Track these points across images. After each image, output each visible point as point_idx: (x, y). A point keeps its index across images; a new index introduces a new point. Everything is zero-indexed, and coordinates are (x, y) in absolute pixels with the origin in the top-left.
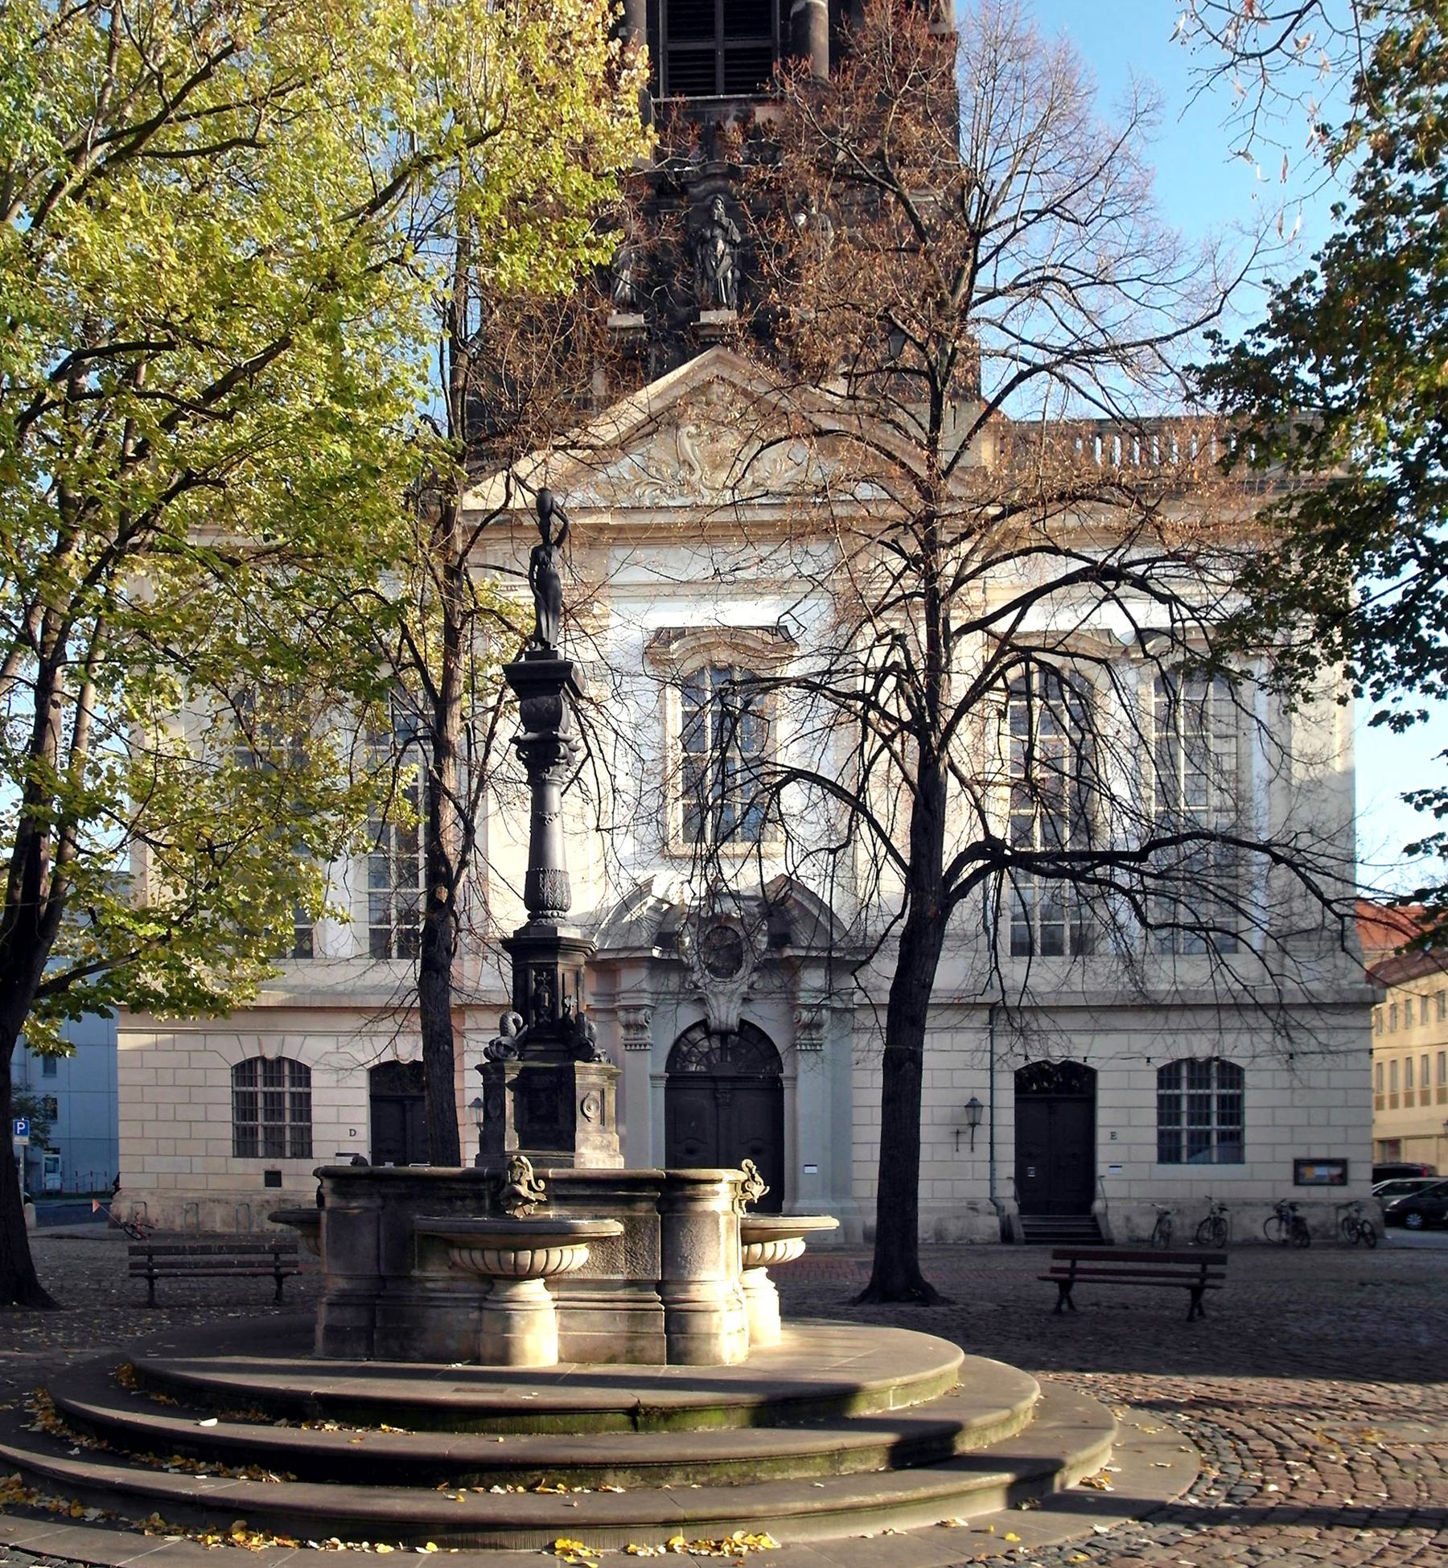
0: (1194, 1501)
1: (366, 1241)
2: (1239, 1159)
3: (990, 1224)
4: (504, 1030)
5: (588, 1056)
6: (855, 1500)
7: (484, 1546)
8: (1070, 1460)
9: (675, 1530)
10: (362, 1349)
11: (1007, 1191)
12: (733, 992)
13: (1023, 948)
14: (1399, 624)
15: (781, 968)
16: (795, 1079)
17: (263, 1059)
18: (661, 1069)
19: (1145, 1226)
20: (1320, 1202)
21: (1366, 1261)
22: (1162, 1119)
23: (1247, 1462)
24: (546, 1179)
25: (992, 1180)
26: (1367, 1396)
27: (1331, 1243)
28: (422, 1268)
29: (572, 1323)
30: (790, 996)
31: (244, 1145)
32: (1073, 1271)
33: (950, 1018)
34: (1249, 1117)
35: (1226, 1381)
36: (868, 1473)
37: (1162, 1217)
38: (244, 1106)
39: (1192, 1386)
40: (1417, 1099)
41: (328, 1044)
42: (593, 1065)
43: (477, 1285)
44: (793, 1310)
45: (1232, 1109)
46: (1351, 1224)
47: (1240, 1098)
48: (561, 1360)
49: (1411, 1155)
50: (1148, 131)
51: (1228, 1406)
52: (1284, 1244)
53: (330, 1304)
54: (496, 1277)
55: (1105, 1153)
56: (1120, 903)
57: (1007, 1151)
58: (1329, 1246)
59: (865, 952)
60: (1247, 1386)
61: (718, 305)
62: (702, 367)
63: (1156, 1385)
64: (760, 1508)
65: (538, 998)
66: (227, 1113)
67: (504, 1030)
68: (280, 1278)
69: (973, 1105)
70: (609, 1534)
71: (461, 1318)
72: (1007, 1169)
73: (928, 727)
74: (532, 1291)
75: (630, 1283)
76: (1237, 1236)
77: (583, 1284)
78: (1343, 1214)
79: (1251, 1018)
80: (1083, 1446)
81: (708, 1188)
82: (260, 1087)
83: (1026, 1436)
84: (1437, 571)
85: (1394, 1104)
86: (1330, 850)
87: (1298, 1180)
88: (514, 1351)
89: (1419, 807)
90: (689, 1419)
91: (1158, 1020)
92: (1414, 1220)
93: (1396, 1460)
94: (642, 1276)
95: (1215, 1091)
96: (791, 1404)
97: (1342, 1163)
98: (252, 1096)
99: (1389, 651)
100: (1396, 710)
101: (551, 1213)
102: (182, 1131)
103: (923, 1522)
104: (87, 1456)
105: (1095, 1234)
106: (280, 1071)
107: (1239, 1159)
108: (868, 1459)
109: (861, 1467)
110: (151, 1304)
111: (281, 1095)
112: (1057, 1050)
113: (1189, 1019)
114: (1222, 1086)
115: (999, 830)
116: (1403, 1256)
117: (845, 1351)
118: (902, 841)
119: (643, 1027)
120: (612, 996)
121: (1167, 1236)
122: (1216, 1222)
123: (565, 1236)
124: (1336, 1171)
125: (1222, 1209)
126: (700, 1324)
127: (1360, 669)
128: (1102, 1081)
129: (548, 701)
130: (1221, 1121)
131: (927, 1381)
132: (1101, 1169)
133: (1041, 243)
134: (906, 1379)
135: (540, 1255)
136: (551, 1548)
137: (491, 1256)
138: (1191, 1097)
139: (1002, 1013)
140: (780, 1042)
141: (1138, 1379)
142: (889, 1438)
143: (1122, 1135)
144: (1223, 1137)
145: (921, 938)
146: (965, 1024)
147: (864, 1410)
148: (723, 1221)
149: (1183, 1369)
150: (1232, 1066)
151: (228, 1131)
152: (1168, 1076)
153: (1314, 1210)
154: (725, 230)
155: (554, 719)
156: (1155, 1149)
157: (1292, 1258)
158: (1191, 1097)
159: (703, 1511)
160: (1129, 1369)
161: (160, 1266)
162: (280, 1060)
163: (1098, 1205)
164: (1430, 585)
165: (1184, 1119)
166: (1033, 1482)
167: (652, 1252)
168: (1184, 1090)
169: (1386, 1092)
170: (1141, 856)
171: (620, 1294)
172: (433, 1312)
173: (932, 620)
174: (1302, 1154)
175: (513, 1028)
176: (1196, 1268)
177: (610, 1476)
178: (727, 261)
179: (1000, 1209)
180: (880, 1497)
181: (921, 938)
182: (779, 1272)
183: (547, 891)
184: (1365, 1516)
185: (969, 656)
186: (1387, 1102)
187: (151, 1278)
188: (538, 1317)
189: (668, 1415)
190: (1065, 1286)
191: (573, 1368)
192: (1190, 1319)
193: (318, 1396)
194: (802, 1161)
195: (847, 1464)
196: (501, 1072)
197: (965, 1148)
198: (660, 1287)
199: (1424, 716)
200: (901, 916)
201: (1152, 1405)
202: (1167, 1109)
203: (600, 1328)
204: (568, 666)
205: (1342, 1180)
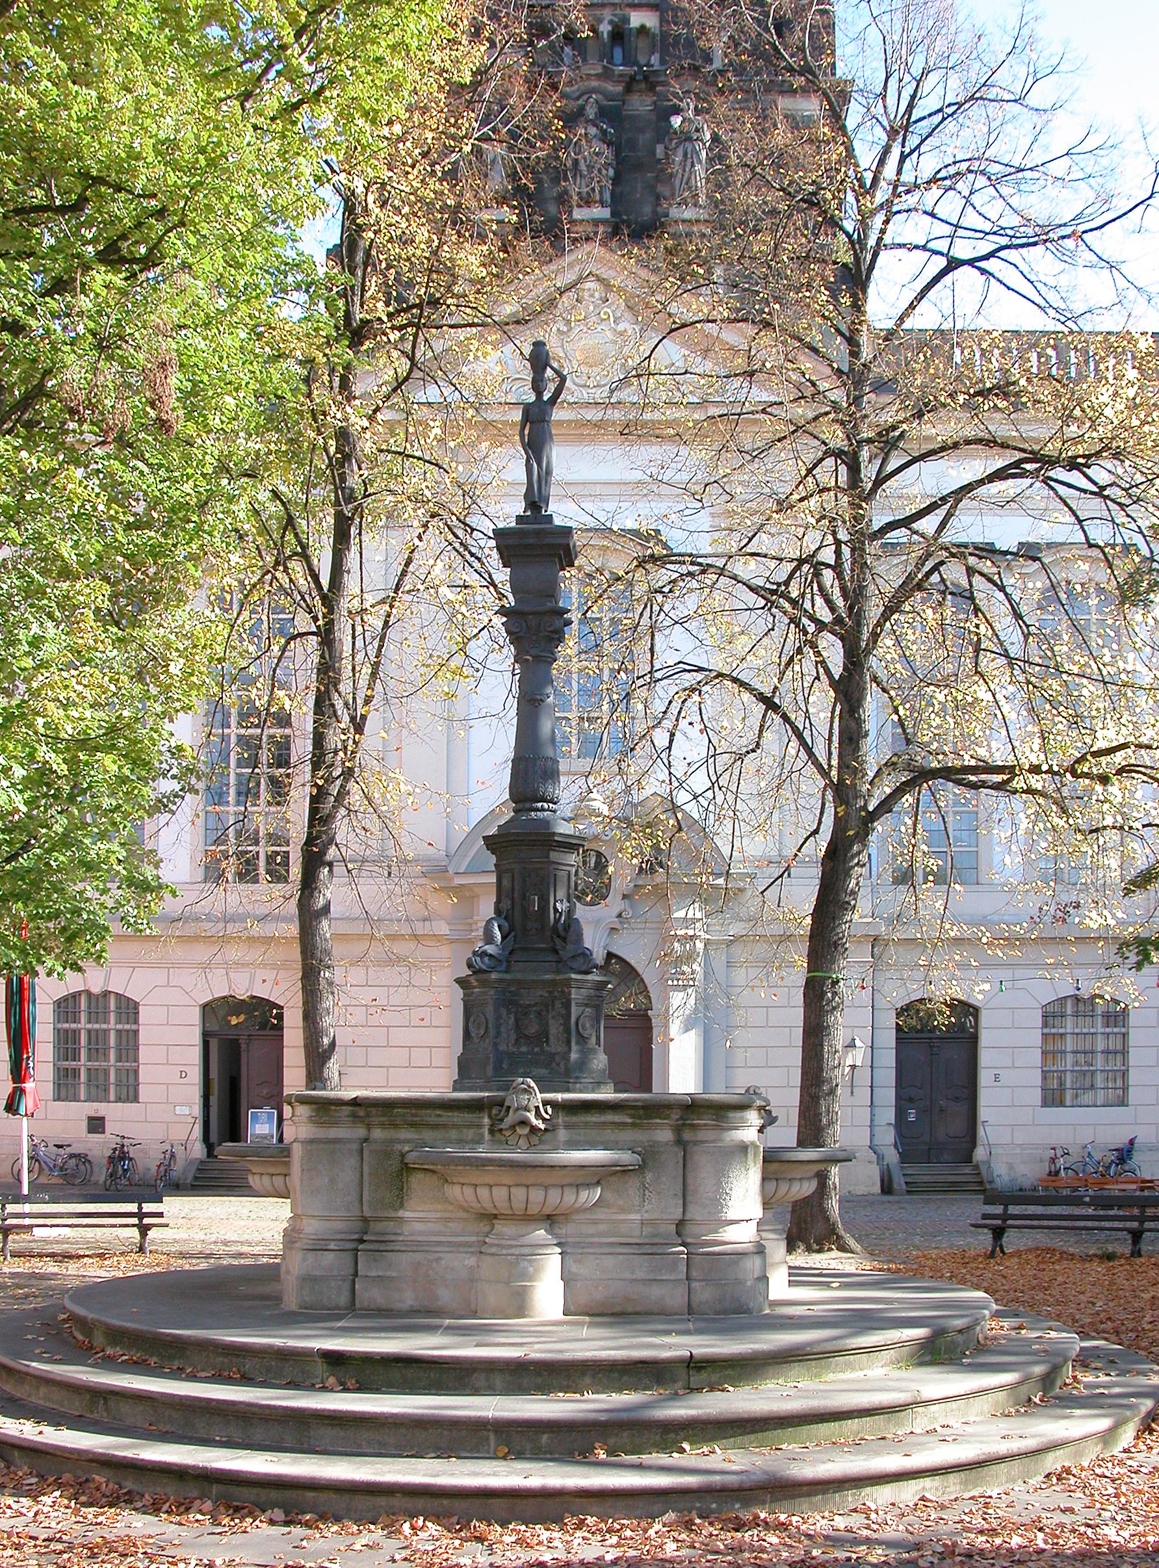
11: (888, 1137)
17: (89, 993)
32: (1005, 1217)
41: (160, 976)
57: (888, 1095)
72: (889, 1115)
82: (83, 1024)
98: (76, 1033)
112: (946, 987)
140: (650, 977)
162: (106, 994)
163: (980, 1153)
179: (880, 1158)
190: (998, 1233)
200: (816, 832)
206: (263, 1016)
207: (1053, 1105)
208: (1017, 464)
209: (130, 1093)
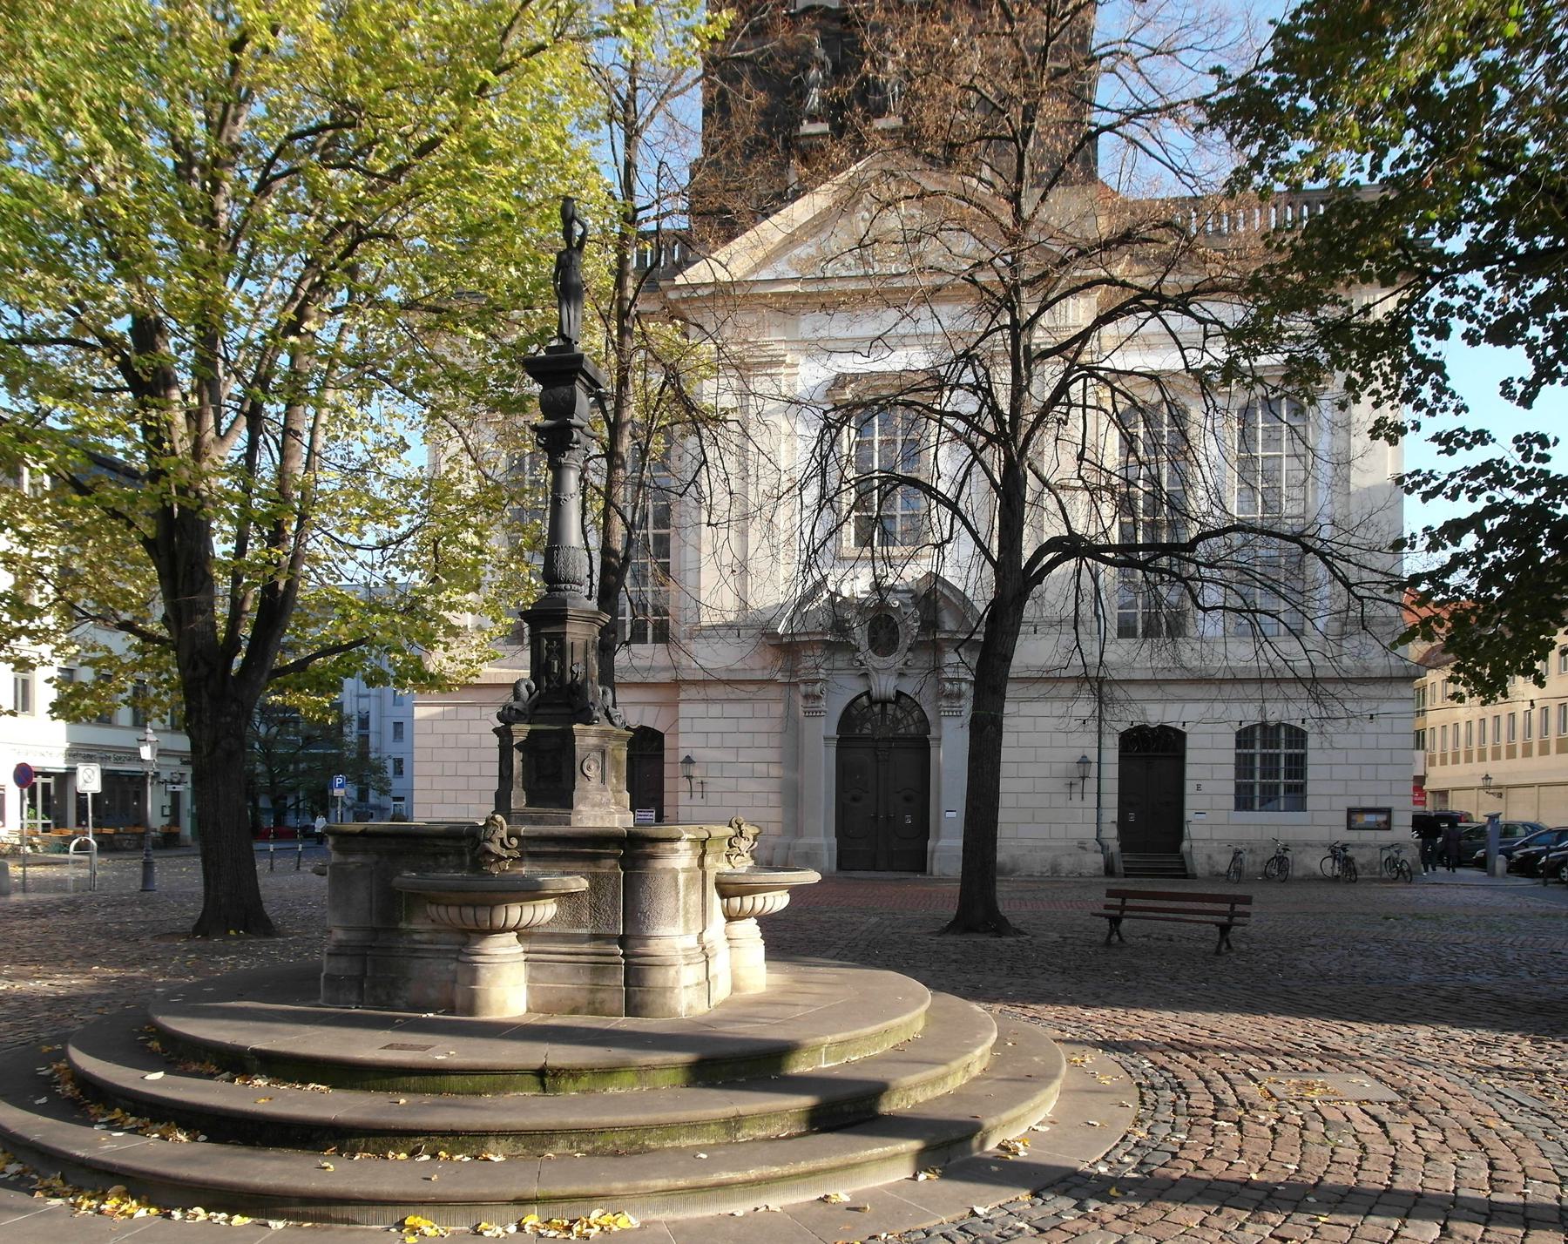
0: (1103, 1169)
2: (1301, 807)
3: (1095, 861)
5: (588, 720)
6: (725, 1176)
7: (337, 1221)
8: (988, 1123)
9: (528, 1208)
10: (353, 997)
11: (1110, 832)
18: (833, 732)
20: (1367, 844)
21: (1404, 893)
22: (1240, 772)
23: (1180, 1120)
24: (519, 837)
26: (1334, 1041)
28: (409, 920)
32: (1123, 908)
34: (1311, 773)
36: (768, 1139)
40: (1504, 753)
42: (593, 728)
45: (1297, 766)
46: (1392, 863)
47: (1304, 756)
48: (529, 1010)
49: (1456, 804)
54: (472, 931)
55: (1192, 802)
57: (1111, 800)
58: (1374, 880)
64: (618, 1186)
65: (549, 665)
69: (1084, 761)
70: (461, 1211)
72: (1111, 814)
75: (595, 937)
76: (1299, 873)
78: (1386, 855)
79: (1291, 690)
81: (668, 846)
84: (1429, 281)
86: (1354, 541)
87: (1349, 828)
88: (480, 1002)
91: (1213, 691)
93: (1325, 1121)
94: (604, 930)
95: (1283, 750)
96: (736, 1062)
103: (803, 1197)
105: (1182, 871)
107: (1301, 807)
108: (769, 1125)
109: (761, 1134)
112: (1157, 714)
113: (1239, 691)
114: (1289, 746)
115: (1079, 527)
119: (818, 698)
120: (793, 672)
121: (1239, 872)
123: (531, 892)
125: (1286, 850)
126: (656, 978)
128: (1190, 742)
129: (565, 390)
130: (1288, 776)
132: (1189, 815)
134: (839, 1037)
136: (401, 1224)
138: (1263, 756)
144: (1289, 789)
146: (1054, 693)
147: (800, 1066)
152: (1244, 737)
157: (1339, 893)
158: (1263, 756)
159: (557, 1190)
163: (1185, 845)
164: (1422, 295)
166: (949, 1146)
167: (614, 906)
168: (1258, 749)
169: (1438, 752)
171: (586, 947)
174: (1354, 803)
176: (1226, 907)
177: (492, 1144)
180: (753, 1173)
183: (560, 565)
184: (1261, 1195)
186: (1438, 760)
188: (506, 969)
190: (1115, 921)
191: (535, 1019)
192: (1218, 952)
193: (254, 1051)
194: (944, 807)
195: (744, 1131)
197: (1077, 797)
198: (623, 941)
202: (1243, 766)
203: (568, 984)
204: (580, 358)
205: (1387, 825)
207: (1245, 809)
208: (1136, 300)
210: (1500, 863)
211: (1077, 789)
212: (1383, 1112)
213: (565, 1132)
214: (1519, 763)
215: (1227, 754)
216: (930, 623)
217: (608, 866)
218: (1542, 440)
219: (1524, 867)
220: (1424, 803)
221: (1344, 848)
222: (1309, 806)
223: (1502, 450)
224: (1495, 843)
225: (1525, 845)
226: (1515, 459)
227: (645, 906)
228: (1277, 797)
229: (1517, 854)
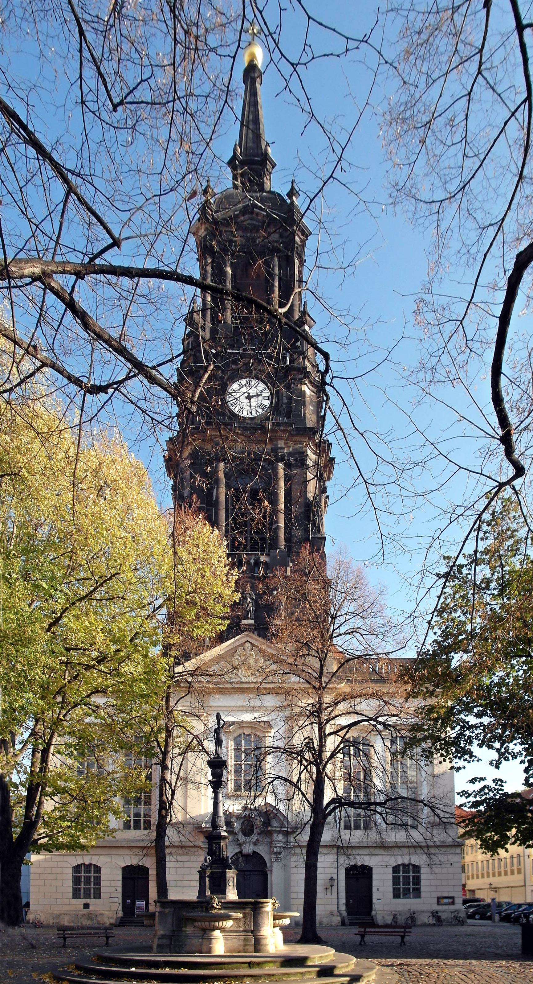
1: (170, 920)
4: (206, 861)
8: (364, 975)
11: (343, 908)
12: (250, 842)
13: (348, 827)
14: (455, 742)
15: (267, 833)
16: (271, 871)
17: (84, 864)
19: (389, 920)
20: (445, 911)
22: (394, 884)
25: (338, 904)
27: (450, 924)
28: (186, 927)
29: (228, 942)
30: (270, 844)
31: (76, 894)
32: (365, 932)
33: (325, 851)
34: (423, 883)
35: (409, 960)
37: (395, 916)
38: (77, 881)
39: (399, 961)
40: (480, 876)
41: (108, 859)
43: (201, 932)
44: (286, 941)
45: (417, 880)
46: (456, 918)
47: (100, 877)
50: (383, 596)
51: (408, 965)
52: (434, 925)
53: (159, 938)
55: (375, 895)
56: (378, 818)
57: (343, 895)
59: (296, 829)
60: (414, 961)
61: (246, 618)
62: (243, 637)
63: (389, 961)
65: (216, 852)
66: (70, 883)
67: (206, 861)
68: (107, 938)
69: (332, 879)
71: (196, 941)
72: (344, 901)
73: (318, 761)
74: (217, 933)
75: (244, 931)
76: (419, 923)
77: (231, 931)
78: (453, 915)
79: (419, 851)
80: (368, 972)
82: (83, 874)
83: (352, 970)
85: (473, 878)
86: (441, 803)
87: (438, 904)
88: (212, 950)
89: (461, 796)
90: (264, 965)
92: (478, 916)
94: (247, 929)
95: (411, 874)
96: (290, 962)
97: (453, 898)
98: (80, 877)
99: (454, 749)
100: (456, 766)
101: (222, 912)
102: (54, 889)
104: (96, 979)
105: (372, 923)
106: (90, 868)
110: (64, 946)
111: (90, 877)
116: (471, 928)
117: (300, 950)
118: (310, 797)
121: (396, 922)
122: (412, 918)
123: (228, 918)
124: (451, 900)
125: (414, 913)
126: (264, 942)
127: (445, 754)
128: (374, 871)
131: (325, 956)
132: (374, 900)
133: (353, 623)
134: (320, 955)
135: (221, 923)
137: (207, 923)
138: (403, 876)
139: (341, 849)
140: (266, 858)
141: (384, 960)
142: (317, 969)
143: (381, 889)
145: (317, 829)
148: (270, 913)
149: (397, 957)
150: (417, 866)
151: (70, 890)
152: (396, 869)
153: (445, 913)
154: (250, 595)
155: (221, 775)
156: (392, 894)
157: (436, 929)
158: (403, 876)
160: (381, 958)
161: (68, 934)
163: (373, 913)
165: (401, 884)
168: (401, 874)
169: (470, 874)
170: (385, 803)
171: (241, 934)
172: (188, 940)
173: (320, 729)
175: (208, 860)
176: (402, 930)
177: (245, 979)
178: (251, 604)
181: (317, 829)
182: (283, 929)
183: (218, 822)
185: (332, 743)
186: (470, 877)
187: (65, 939)
188: (219, 940)
189: (259, 964)
190: (363, 936)
191: (229, 954)
192: (401, 945)
196: (205, 873)
198: (252, 932)
199: (464, 767)
201: (387, 966)
202: (396, 880)
203: (236, 943)
205: (453, 903)
206: (142, 871)
209: (98, 895)
210: (497, 918)
211: (329, 890)
212: (466, 973)
213: (264, 975)
214: (503, 878)
215: (390, 876)
216: (267, 823)
217: (248, 911)
218: (501, 781)
219: (506, 919)
220: (465, 895)
221: (437, 912)
222: (422, 896)
223: (489, 782)
224: (494, 909)
225: (506, 910)
226: (493, 785)
227: (260, 921)
228: (409, 893)
229: (503, 914)
